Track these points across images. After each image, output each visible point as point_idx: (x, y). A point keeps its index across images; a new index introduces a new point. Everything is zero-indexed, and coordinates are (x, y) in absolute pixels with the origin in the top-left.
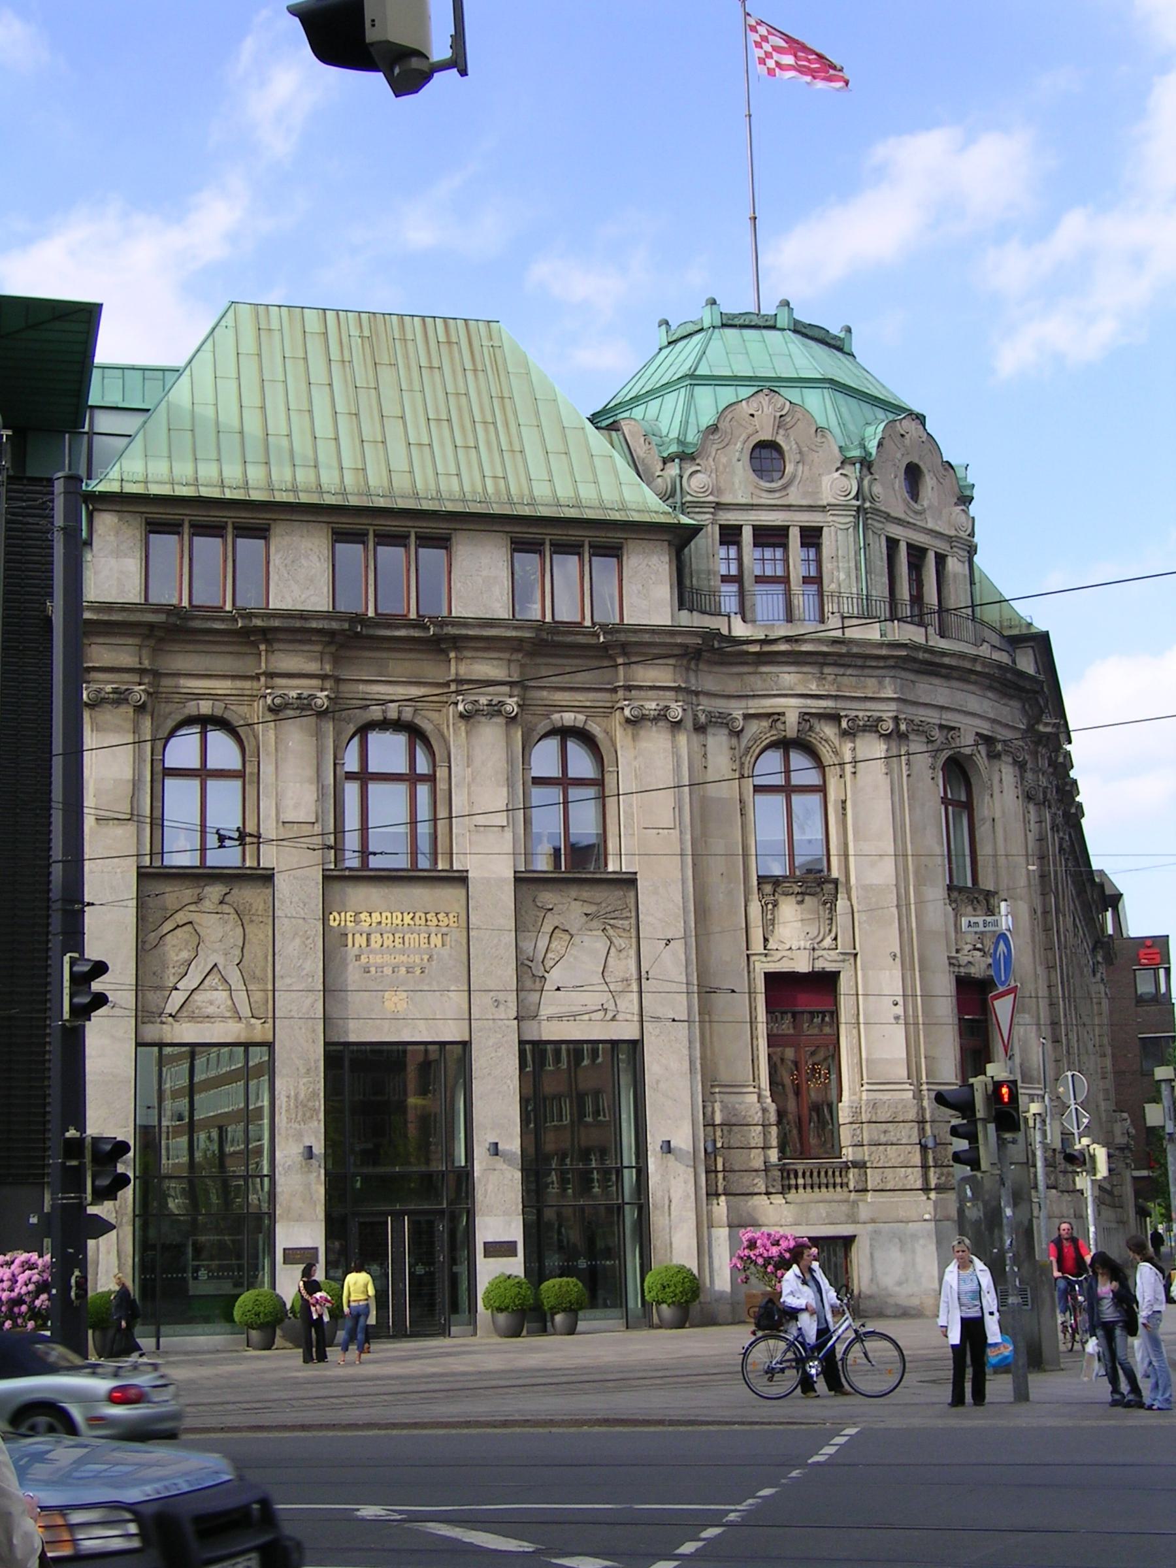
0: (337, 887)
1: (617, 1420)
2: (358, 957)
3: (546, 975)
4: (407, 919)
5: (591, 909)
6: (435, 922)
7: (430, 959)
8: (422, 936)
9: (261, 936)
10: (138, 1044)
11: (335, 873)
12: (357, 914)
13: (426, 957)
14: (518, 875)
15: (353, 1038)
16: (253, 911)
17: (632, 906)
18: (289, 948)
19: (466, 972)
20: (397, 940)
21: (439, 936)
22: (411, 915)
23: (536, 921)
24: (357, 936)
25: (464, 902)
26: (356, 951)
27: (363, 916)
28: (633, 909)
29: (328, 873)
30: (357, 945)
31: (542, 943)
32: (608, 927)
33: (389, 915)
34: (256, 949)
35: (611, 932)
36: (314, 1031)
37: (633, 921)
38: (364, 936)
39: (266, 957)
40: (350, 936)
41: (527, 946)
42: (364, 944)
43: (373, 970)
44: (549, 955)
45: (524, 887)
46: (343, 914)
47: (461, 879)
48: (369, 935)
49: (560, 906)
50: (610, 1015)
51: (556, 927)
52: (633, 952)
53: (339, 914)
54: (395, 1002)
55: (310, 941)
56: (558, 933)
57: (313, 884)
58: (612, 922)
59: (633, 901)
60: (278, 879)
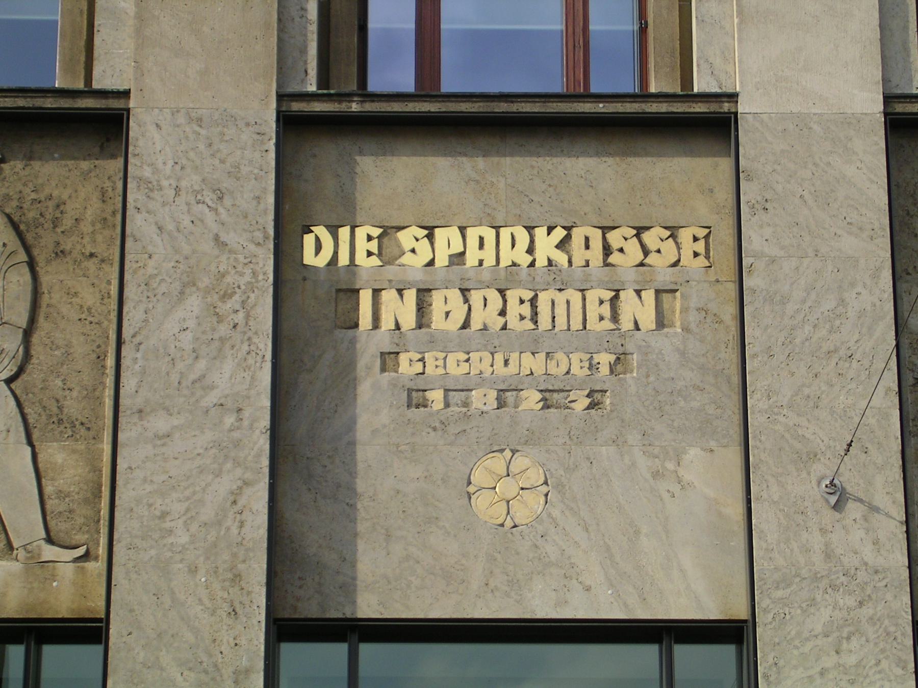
0: (325, 152)
1: (351, 244)
2: (388, 359)
4: (546, 245)
6: (634, 252)
7: (620, 361)
8: (593, 296)
9: (89, 297)
10: (284, 629)
11: (318, 107)
12: (388, 231)
13: (605, 359)
15: (360, 615)
16: (67, 222)
18: (166, 325)
19: (736, 398)
20: (514, 309)
21: (649, 296)
22: (559, 233)
24: (390, 296)
25: (725, 195)
26: (383, 340)
27: (406, 238)
29: (296, 106)
30: (387, 323)
33: (489, 235)
34: (69, 334)
36: (237, 578)
38: (411, 296)
39: (101, 358)
40: (366, 297)
42: (409, 319)
43: (436, 396)
46: (344, 232)
47: (711, 125)
48: (424, 294)
53: (334, 231)
54: (506, 488)
55: (234, 302)
57: (247, 136)
60: (147, 133)
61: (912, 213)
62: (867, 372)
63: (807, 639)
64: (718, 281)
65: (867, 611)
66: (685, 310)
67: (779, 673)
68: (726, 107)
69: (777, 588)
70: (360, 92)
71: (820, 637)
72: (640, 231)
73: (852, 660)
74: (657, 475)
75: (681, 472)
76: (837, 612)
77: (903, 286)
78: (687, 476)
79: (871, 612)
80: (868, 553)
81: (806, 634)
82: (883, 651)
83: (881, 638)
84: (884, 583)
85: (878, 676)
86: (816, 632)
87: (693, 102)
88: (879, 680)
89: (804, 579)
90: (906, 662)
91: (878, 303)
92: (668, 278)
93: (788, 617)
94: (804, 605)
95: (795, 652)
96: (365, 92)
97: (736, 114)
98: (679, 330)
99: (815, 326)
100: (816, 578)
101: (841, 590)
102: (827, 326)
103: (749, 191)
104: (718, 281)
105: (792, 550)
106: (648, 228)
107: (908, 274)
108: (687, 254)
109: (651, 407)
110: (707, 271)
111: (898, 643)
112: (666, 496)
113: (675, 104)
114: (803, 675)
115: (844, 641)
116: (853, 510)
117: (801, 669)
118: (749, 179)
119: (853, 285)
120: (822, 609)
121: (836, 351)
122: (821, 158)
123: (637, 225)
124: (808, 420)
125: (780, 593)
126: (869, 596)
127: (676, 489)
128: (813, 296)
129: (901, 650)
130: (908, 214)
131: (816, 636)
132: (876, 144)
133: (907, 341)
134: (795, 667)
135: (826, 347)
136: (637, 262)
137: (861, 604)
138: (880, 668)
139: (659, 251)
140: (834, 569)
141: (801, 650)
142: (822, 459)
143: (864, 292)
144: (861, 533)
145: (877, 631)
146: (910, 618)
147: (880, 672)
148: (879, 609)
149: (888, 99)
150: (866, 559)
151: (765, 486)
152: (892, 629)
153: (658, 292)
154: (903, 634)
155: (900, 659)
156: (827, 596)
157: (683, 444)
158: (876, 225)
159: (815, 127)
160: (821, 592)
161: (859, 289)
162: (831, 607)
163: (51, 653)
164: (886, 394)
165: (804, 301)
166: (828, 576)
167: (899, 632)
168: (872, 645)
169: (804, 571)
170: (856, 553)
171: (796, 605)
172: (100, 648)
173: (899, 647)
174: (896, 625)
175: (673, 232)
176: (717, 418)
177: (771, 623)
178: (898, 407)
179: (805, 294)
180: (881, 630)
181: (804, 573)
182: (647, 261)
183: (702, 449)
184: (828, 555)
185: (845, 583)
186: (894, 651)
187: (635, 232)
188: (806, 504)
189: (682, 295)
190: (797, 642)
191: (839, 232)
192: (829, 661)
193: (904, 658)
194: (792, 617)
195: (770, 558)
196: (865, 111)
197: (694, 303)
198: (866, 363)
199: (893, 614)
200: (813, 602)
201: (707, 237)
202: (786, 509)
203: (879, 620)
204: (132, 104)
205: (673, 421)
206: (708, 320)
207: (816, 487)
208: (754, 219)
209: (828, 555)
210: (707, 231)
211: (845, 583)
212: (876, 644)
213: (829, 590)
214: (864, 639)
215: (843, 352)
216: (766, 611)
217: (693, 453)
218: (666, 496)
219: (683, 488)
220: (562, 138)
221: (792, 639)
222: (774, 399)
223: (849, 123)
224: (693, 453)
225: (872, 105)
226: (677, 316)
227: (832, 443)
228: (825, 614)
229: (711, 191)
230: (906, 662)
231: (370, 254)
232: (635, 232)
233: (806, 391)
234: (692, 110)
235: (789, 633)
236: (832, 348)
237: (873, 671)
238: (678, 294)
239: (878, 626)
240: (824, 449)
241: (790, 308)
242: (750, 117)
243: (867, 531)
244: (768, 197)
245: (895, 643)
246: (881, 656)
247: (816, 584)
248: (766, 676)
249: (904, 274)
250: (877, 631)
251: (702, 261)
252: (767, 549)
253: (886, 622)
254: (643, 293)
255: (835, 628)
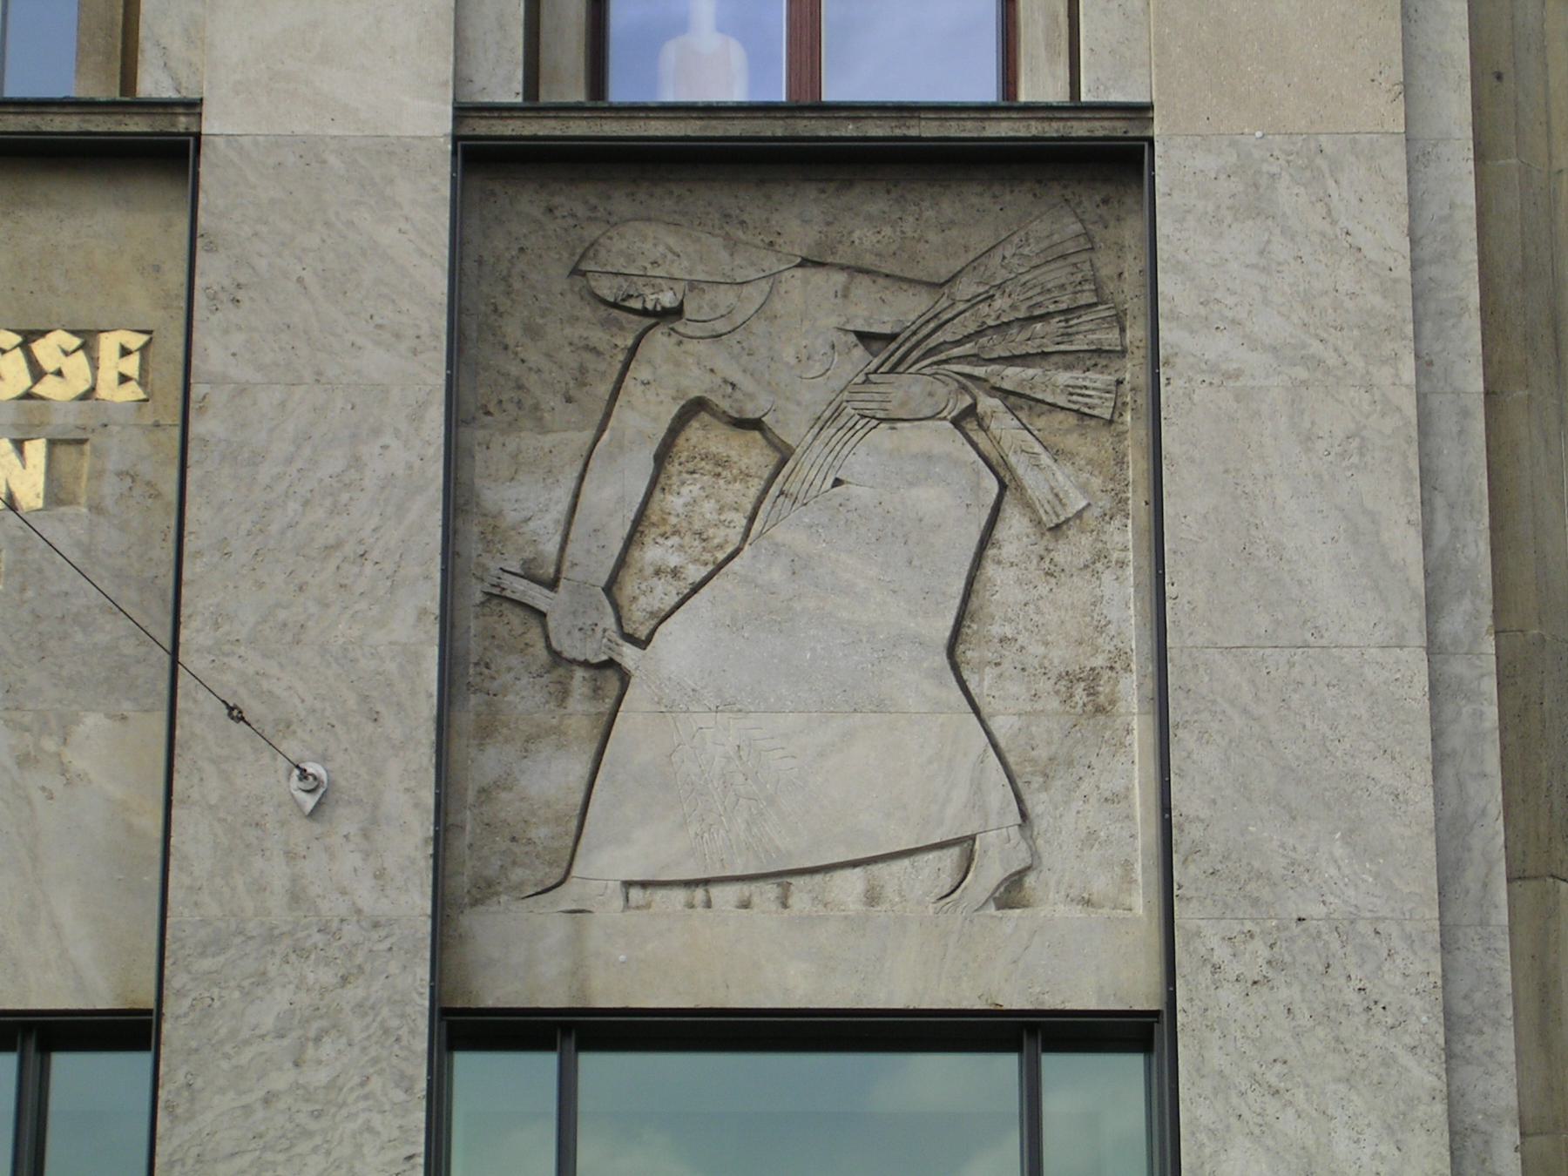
3: (629, 656)
5: (896, 310)
14: (482, 127)
15: (489, 1002)
17: (1130, 295)
21: (36, 450)
23: (581, 377)
28: (1135, 305)
31: (616, 489)
32: (987, 403)
35: (1004, 426)
37: (1133, 371)
41: (527, 504)
44: (653, 553)
45: (530, 215)
47: (155, 152)
49: (726, 297)
50: (990, 873)
51: (695, 408)
52: (1126, 538)
56: (702, 437)
58: (1012, 376)
59: (1133, 266)
61: (501, 309)
62: (389, 583)
63: (247, 1042)
64: (157, 425)
65: (355, 992)
66: (97, 475)
67: (192, 1100)
68: (183, 123)
69: (203, 954)
70: (528, 104)
71: (268, 1039)
72: (29, 337)
73: (322, 1076)
74: (25, 760)
75: (68, 755)
76: (303, 994)
77: (472, 436)
78: (78, 762)
79: (361, 993)
80: (364, 894)
81: (245, 1033)
82: (375, 1061)
83: (374, 1039)
84: (387, 944)
85: (362, 1104)
86: (263, 1031)
87: (124, 114)
88: (363, 1110)
89: (252, 938)
90: (412, 1079)
91: (418, 463)
92: (71, 420)
93: (217, 1004)
94: (246, 983)
95: (225, 1065)
96: (600, 104)
97: (198, 136)
98: (84, 510)
99: (306, 503)
100: (271, 937)
101: (313, 957)
102: (328, 502)
103: (211, 271)
104: (157, 425)
105: (233, 889)
106: (43, 333)
107: (488, 413)
108: (108, 375)
109: (24, 644)
110: (140, 409)
111: (401, 1048)
112: (38, 796)
113: (93, 118)
114: (234, 1104)
115: (311, 1044)
116: (346, 821)
117: (231, 1094)
118: (212, 248)
119: (376, 432)
120: (277, 990)
121: (338, 545)
122: (337, 214)
123: (24, 327)
124: (281, 665)
125: (207, 964)
126: (360, 967)
127: (56, 784)
128: (307, 451)
129: (406, 1059)
130: (496, 310)
131: (262, 1037)
132: (435, 190)
133: (476, 529)
134: (222, 1091)
135: (326, 537)
136: (20, 391)
137: (345, 980)
138: (367, 1089)
139: (59, 373)
140: (304, 921)
141: (234, 1062)
142: (299, 731)
143: (394, 444)
144: (356, 859)
145: (368, 1027)
146: (427, 1003)
147: (366, 1097)
148: (374, 989)
149: (462, 112)
150: (360, 903)
151: (196, 780)
152: (395, 1023)
153: (52, 444)
154: (412, 1032)
155: (403, 1076)
156: (287, 968)
157: (75, 707)
158: (425, 329)
159: (333, 160)
160: (277, 961)
161: (387, 439)
162: (292, 987)
163: (67, 1068)
164: (419, 619)
165: (290, 460)
166: (291, 933)
167: (405, 1029)
168: (356, 1050)
169: (251, 925)
170: (344, 893)
171: (232, 984)
172: (145, 1058)
173: (402, 1054)
174: (402, 1016)
175: (88, 341)
176: (138, 662)
177: (186, 1015)
178: (437, 641)
179: (292, 449)
180: (375, 1025)
181: (252, 927)
182: (39, 389)
183: (108, 716)
184: (296, 897)
185: (321, 945)
186: (395, 1061)
187: (18, 339)
188: (265, 809)
189: (95, 450)
190: (228, 1048)
191: (360, 341)
192: (280, 1081)
193: (409, 1071)
194: (223, 1005)
195: (196, 904)
196: (419, 133)
197: (112, 463)
198: (388, 567)
199: (397, 997)
200: (262, 979)
201: (144, 349)
202: (230, 818)
203: (372, 1008)
204: (1157, 130)
205: (61, 667)
206: (137, 492)
207: (283, 780)
208: (215, 319)
209: (296, 897)
210: (145, 338)
211: (321, 945)
212: (364, 1049)
213: (293, 957)
214: (344, 1040)
215: (349, 549)
216: (180, 994)
217: (92, 723)
218: (38, 796)
219: (69, 783)
220: (850, 184)
221: (221, 1042)
222: (226, 628)
223: (391, 154)
224: (92, 723)
225: (439, 124)
226: (83, 484)
227: (318, 705)
228: (281, 998)
229: (157, 269)
230: (412, 1079)
231: (124, 379)
232: (18, 339)
233: (282, 615)
234: (122, 129)
235: (216, 1032)
236: (332, 541)
237: (355, 1095)
238: (87, 447)
239: (369, 1019)
240: (303, 714)
241: (265, 473)
242: (220, 142)
243: (367, 855)
244: (242, 280)
245: (396, 1047)
246: (371, 1070)
247: (270, 948)
248: (171, 1108)
249: (480, 414)
250: (368, 1027)
251: (132, 392)
252: (190, 888)
253: (385, 1012)
254: (28, 445)
255: (295, 1022)
